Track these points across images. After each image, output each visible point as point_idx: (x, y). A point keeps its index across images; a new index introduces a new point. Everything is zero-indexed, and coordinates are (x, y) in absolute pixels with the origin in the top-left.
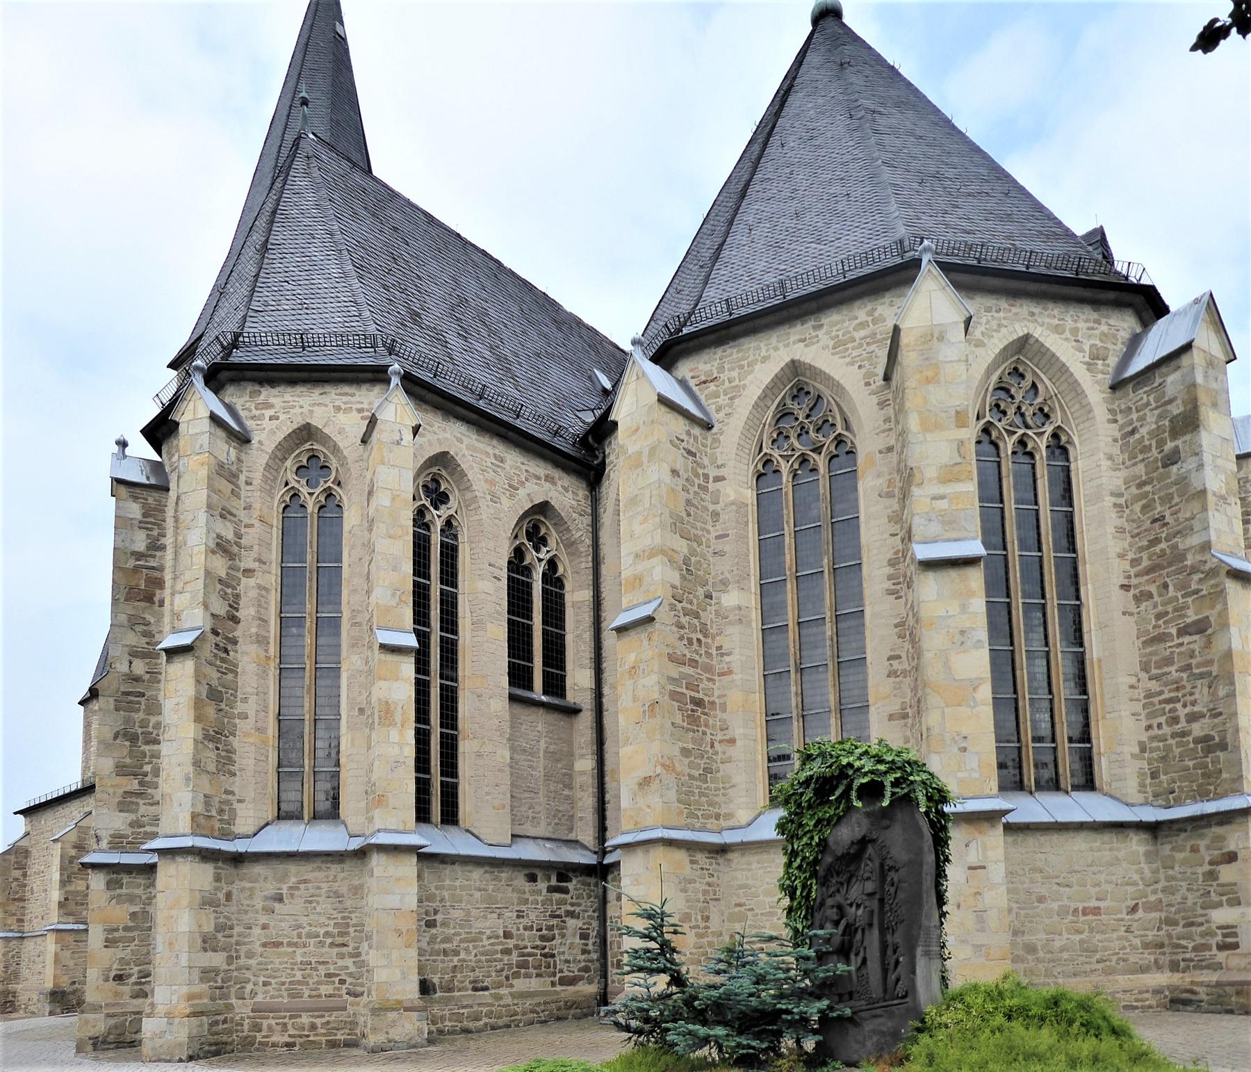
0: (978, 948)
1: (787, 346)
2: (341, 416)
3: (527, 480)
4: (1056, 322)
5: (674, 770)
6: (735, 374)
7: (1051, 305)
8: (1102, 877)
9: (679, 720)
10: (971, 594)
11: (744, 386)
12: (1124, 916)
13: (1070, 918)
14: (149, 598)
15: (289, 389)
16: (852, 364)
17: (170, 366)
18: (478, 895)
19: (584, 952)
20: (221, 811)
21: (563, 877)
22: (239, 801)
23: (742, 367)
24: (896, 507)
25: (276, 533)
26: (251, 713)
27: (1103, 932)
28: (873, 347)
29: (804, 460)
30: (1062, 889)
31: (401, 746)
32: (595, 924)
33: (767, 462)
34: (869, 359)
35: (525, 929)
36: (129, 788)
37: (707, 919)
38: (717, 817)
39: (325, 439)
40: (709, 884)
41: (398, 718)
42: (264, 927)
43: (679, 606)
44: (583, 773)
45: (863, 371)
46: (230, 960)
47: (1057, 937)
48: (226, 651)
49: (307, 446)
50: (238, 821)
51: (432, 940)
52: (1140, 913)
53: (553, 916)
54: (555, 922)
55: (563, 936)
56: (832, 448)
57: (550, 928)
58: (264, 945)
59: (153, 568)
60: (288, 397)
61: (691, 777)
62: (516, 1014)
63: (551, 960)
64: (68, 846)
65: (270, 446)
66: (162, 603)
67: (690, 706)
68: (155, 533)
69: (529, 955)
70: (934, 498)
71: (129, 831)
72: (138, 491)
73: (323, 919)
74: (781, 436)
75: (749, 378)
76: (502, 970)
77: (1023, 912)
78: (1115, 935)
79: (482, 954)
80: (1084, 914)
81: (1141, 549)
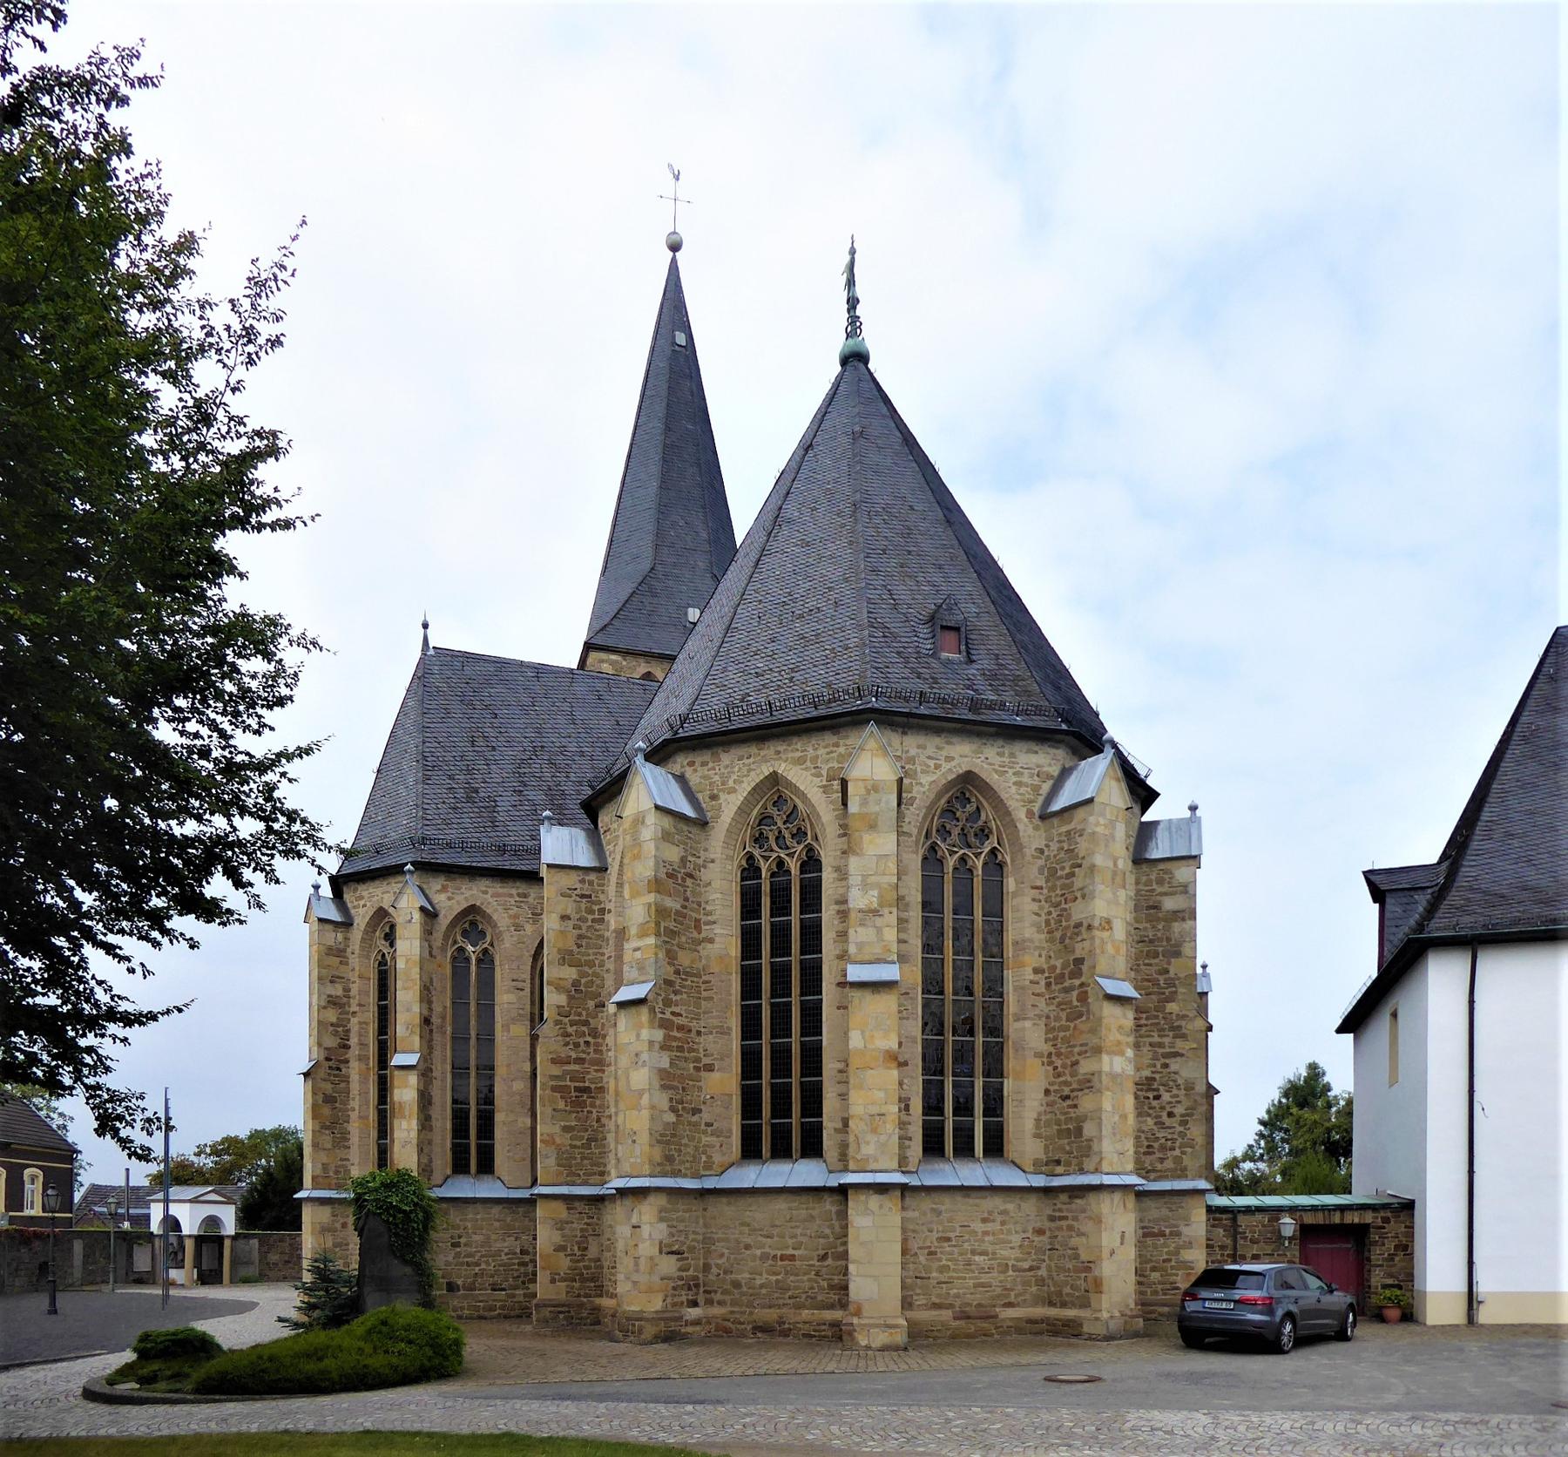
0: (635, 1283)
4: (799, 754)
7: (795, 739)
9: (561, 1105)
12: (814, 1262)
18: (497, 1224)
20: (337, 1172)
33: (750, 858)
48: (339, 1069)
51: (458, 1255)
52: (829, 1261)
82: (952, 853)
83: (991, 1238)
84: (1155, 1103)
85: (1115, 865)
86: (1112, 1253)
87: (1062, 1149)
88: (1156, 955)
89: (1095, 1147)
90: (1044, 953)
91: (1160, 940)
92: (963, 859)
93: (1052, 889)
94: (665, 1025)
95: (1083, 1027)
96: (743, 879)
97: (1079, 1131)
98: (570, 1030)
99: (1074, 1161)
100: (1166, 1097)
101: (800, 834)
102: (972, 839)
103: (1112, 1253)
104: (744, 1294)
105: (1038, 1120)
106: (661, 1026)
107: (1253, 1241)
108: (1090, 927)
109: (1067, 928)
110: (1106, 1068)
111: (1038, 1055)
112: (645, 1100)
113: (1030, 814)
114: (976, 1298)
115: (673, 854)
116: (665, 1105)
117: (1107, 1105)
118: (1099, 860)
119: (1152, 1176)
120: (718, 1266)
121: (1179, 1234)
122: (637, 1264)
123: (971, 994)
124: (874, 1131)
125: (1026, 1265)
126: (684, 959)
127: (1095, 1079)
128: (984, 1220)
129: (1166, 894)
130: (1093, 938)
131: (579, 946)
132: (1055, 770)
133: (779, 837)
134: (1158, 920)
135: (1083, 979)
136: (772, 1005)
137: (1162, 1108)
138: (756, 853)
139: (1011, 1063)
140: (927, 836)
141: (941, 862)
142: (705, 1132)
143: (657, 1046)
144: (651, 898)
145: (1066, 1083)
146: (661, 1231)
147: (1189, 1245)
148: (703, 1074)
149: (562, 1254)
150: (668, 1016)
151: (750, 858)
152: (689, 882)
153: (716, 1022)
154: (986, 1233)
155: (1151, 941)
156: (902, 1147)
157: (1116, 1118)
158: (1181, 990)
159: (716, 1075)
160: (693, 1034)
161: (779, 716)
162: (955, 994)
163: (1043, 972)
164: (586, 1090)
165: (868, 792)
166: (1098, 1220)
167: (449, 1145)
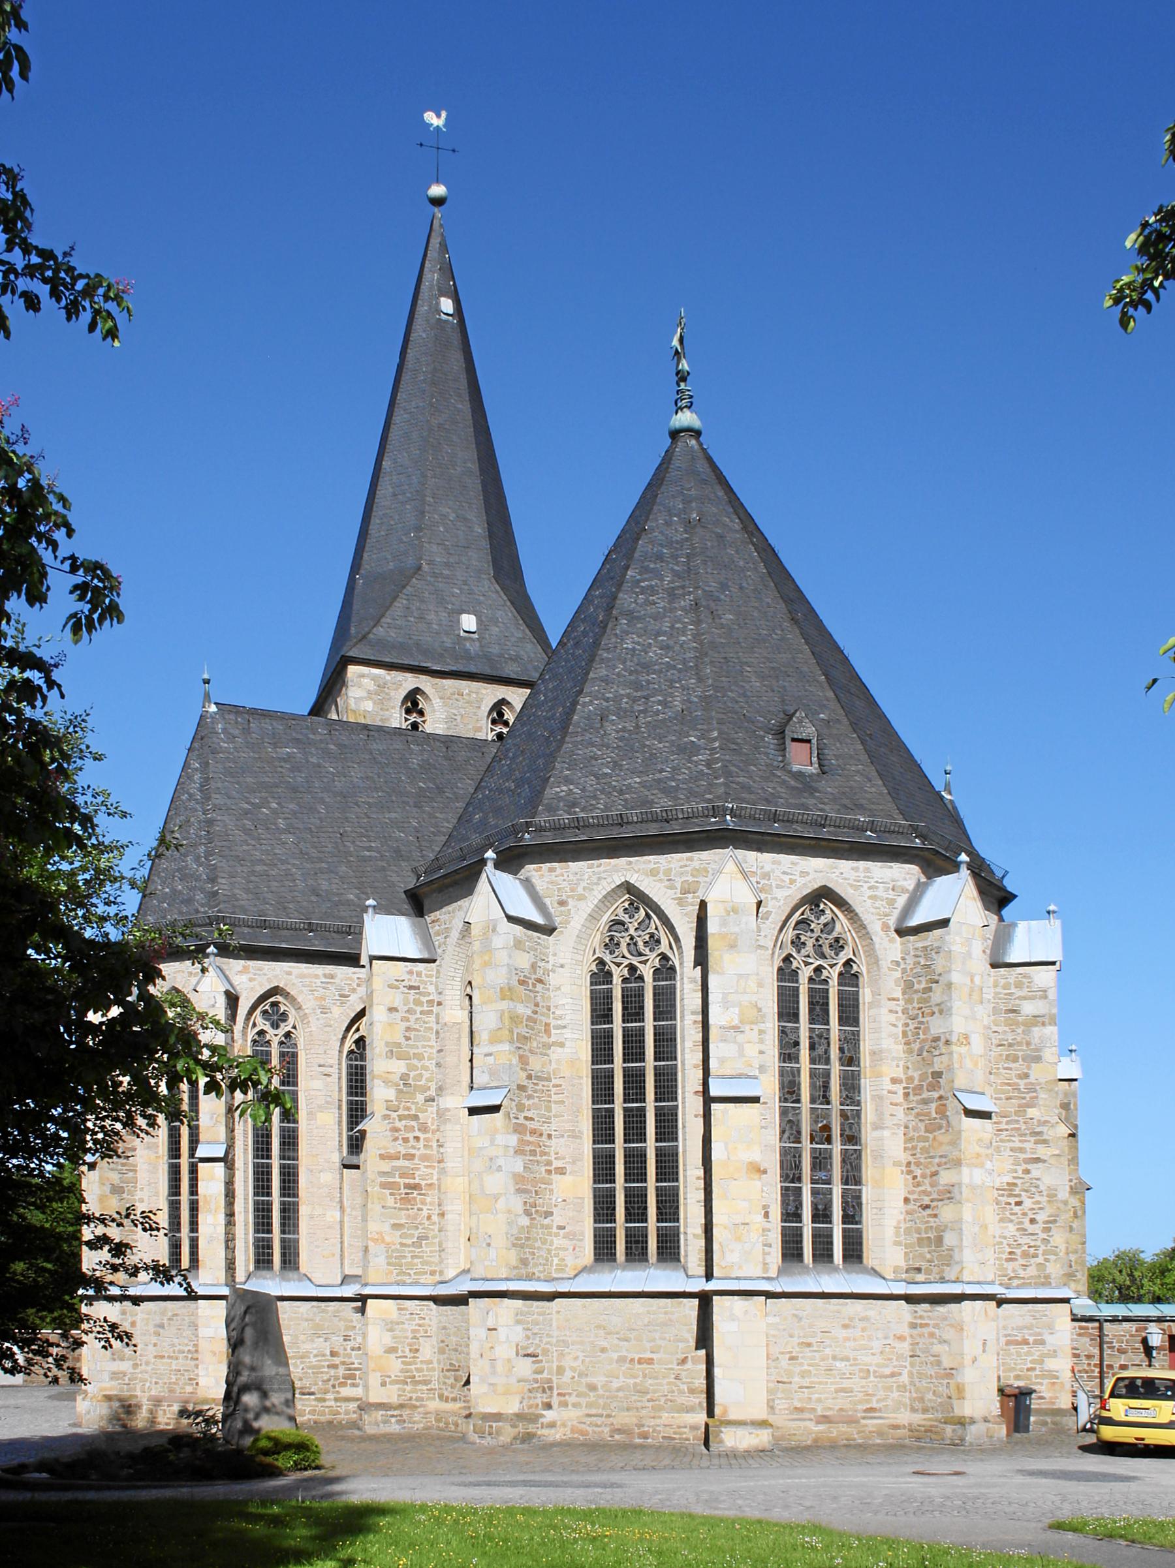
3: (358, 985)
5: (383, 1241)
8: (657, 1335)
9: (390, 1201)
13: (627, 1365)
26: (146, 1198)
27: (656, 1378)
29: (632, 968)
30: (622, 1343)
31: (215, 1226)
33: (601, 962)
38: (433, 1273)
41: (213, 1206)
42: (155, 1345)
43: (394, 1115)
46: (135, 1366)
47: (615, 1380)
58: (155, 1357)
70: (486, 1055)
72: (488, 671)
73: (186, 1341)
76: (329, 1380)
77: (588, 1359)
78: (665, 1382)
79: (309, 1368)
80: (640, 1362)
83: (852, 1344)
84: (1017, 1209)
85: (972, 980)
86: (974, 1360)
87: (922, 1256)
88: (1015, 1060)
89: (957, 1257)
90: (901, 1063)
91: (1020, 1044)
92: (818, 970)
93: (909, 1001)
94: (519, 1129)
95: (941, 1138)
96: (592, 984)
97: (939, 1240)
98: (398, 1124)
99: (935, 1270)
100: (1028, 1203)
102: (826, 950)
103: (974, 1360)
104: (599, 1397)
105: (897, 1228)
106: (515, 1131)
107: (1121, 1351)
108: (947, 1042)
109: (924, 1040)
110: (966, 1180)
111: (896, 1164)
112: (501, 1204)
113: (885, 927)
114: (842, 1402)
115: (523, 961)
116: (520, 1209)
117: (967, 1214)
118: (955, 977)
119: (1015, 1282)
120: (573, 1369)
121: (1042, 1342)
122: (493, 1367)
123: (828, 1103)
124: (738, 1239)
125: (887, 1371)
126: (535, 1064)
127: (956, 1190)
128: (845, 1326)
129: (1025, 998)
130: (951, 1053)
131: (408, 1039)
132: (910, 885)
133: (633, 942)
134: (1017, 1024)
135: (942, 1092)
136: (625, 1109)
137: (1025, 1214)
138: (607, 958)
139: (868, 1171)
141: (795, 973)
142: (557, 1235)
143: (512, 1151)
144: (504, 1005)
145: (925, 1193)
146: (518, 1334)
147: (1054, 1354)
148: (554, 1177)
149: (393, 1356)
150: (521, 1121)
151: (601, 962)
152: (539, 987)
153: (568, 1126)
154: (847, 1339)
155: (1010, 1045)
156: (765, 1254)
157: (976, 1229)
158: (1042, 1095)
159: (568, 1179)
160: (544, 1138)
162: (813, 1101)
163: (901, 1081)
164: (416, 1187)
165: (728, 914)
166: (959, 1328)
167: (251, 1241)
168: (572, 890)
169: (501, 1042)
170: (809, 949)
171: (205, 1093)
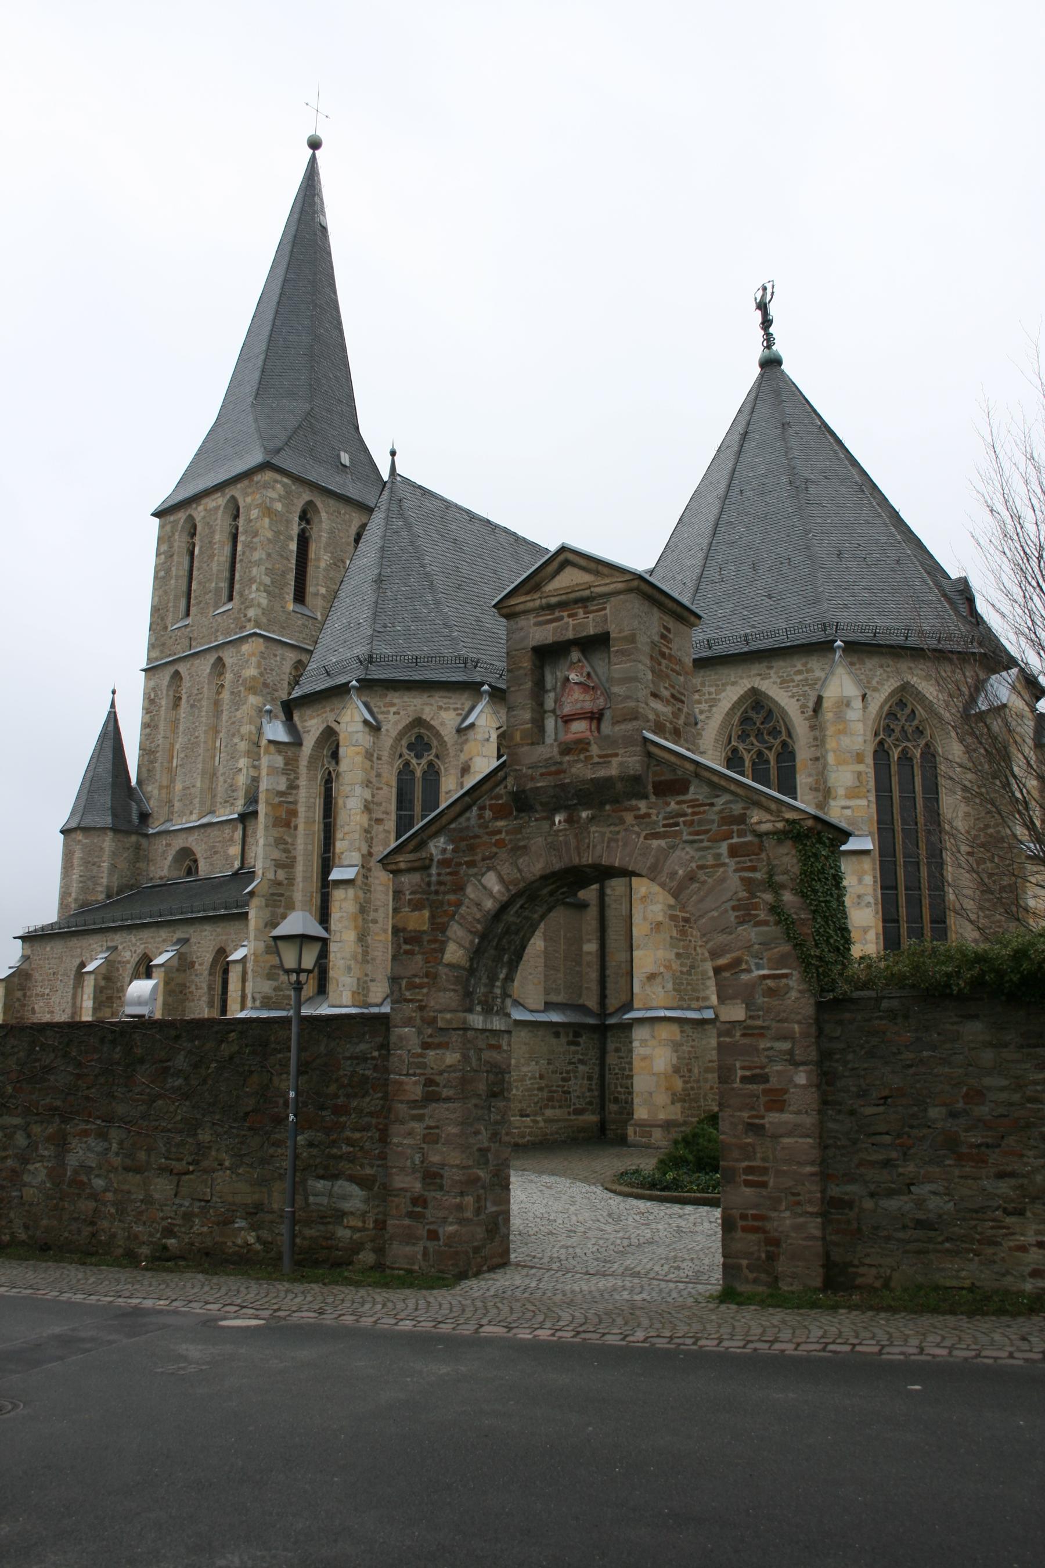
1: (750, 676)
2: (443, 714)
6: (713, 689)
9: (675, 934)
10: (864, 872)
11: (719, 700)
14: (287, 824)
15: (407, 693)
16: (793, 697)
17: (154, 515)
19: (590, 1090)
21: (577, 1035)
22: (372, 981)
23: (717, 686)
24: (821, 798)
25: (394, 791)
26: (380, 920)
28: (806, 688)
29: (760, 754)
32: (597, 1069)
33: (735, 750)
34: (804, 695)
35: (553, 1072)
36: (273, 963)
37: (690, 1071)
38: (698, 999)
39: (430, 727)
40: (692, 1047)
44: (589, 953)
45: (800, 703)
49: (416, 730)
50: (371, 994)
53: (570, 1063)
54: (571, 1067)
55: (576, 1077)
56: (779, 748)
57: (568, 1072)
59: (290, 802)
60: (406, 699)
61: (682, 972)
62: (546, 1134)
63: (568, 1096)
64: (100, 977)
65: (394, 733)
66: (296, 828)
67: (681, 924)
68: (292, 777)
69: (555, 1092)
71: (273, 994)
72: (281, 747)
74: (743, 737)
75: (723, 694)
81: (980, 830)
82: (896, 746)
92: (904, 751)
101: (775, 732)
140: (876, 734)
161: (755, 646)
168: (868, 682)
169: (859, 797)
170: (897, 733)
171: (740, 877)
